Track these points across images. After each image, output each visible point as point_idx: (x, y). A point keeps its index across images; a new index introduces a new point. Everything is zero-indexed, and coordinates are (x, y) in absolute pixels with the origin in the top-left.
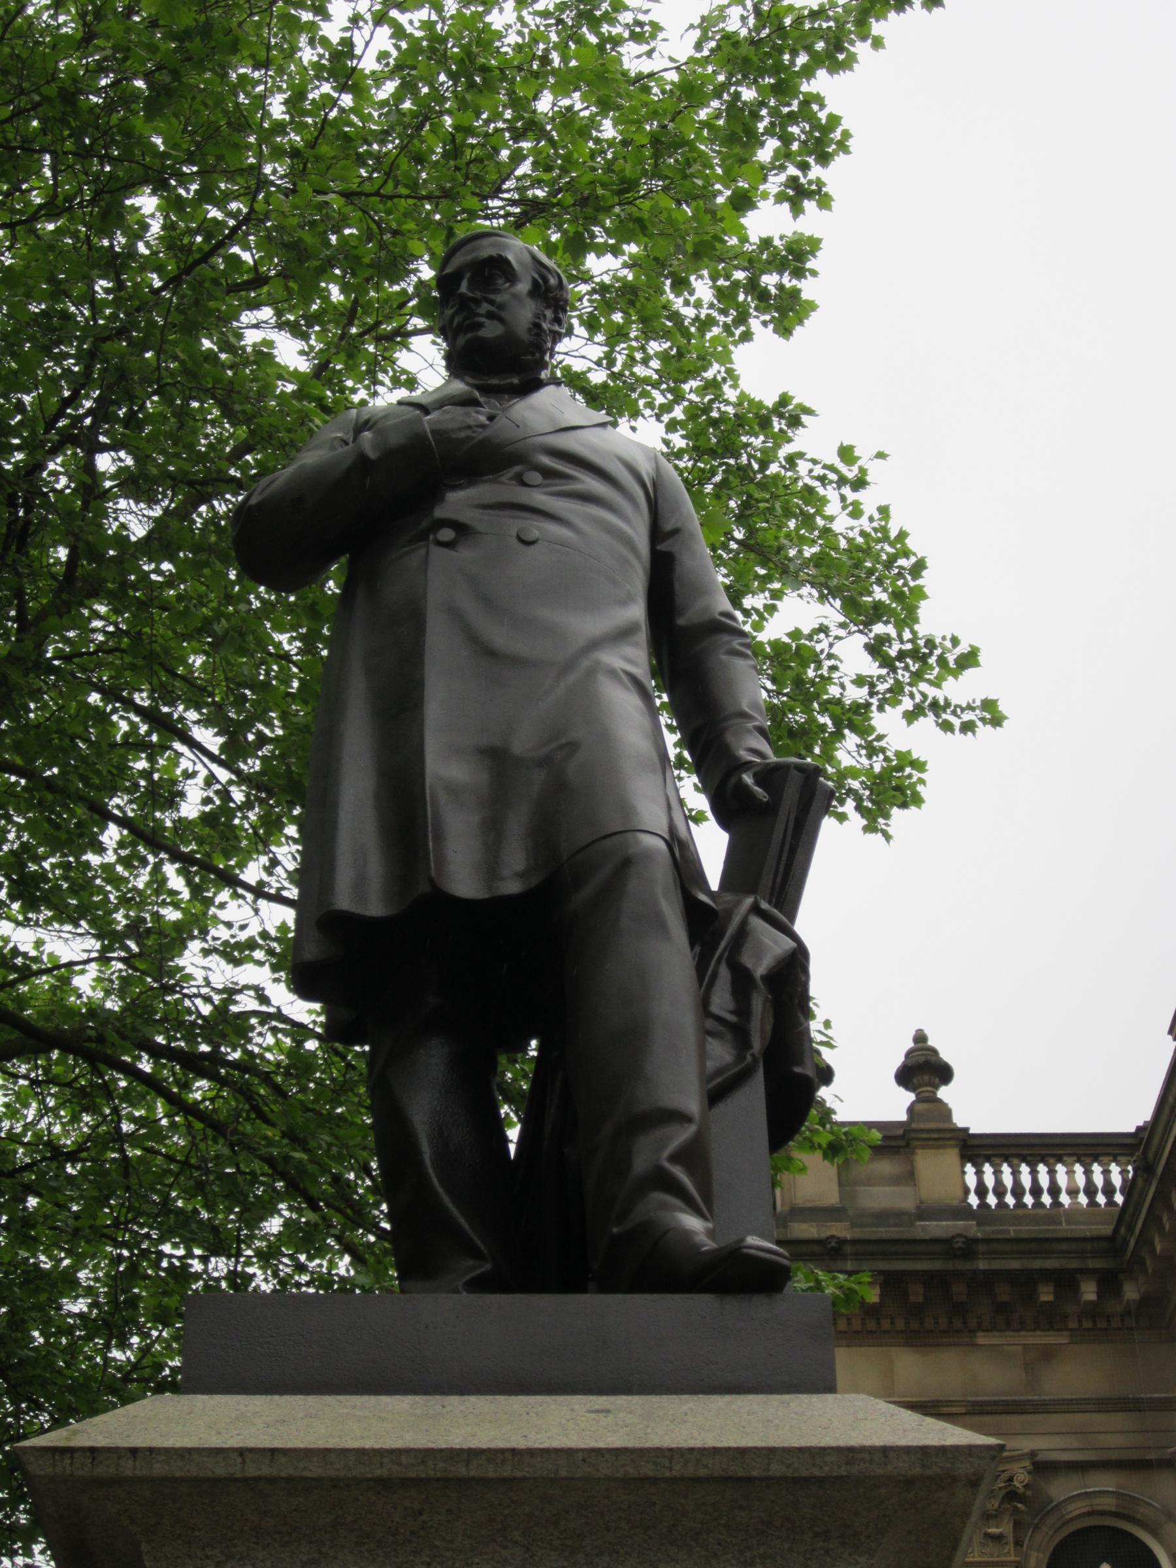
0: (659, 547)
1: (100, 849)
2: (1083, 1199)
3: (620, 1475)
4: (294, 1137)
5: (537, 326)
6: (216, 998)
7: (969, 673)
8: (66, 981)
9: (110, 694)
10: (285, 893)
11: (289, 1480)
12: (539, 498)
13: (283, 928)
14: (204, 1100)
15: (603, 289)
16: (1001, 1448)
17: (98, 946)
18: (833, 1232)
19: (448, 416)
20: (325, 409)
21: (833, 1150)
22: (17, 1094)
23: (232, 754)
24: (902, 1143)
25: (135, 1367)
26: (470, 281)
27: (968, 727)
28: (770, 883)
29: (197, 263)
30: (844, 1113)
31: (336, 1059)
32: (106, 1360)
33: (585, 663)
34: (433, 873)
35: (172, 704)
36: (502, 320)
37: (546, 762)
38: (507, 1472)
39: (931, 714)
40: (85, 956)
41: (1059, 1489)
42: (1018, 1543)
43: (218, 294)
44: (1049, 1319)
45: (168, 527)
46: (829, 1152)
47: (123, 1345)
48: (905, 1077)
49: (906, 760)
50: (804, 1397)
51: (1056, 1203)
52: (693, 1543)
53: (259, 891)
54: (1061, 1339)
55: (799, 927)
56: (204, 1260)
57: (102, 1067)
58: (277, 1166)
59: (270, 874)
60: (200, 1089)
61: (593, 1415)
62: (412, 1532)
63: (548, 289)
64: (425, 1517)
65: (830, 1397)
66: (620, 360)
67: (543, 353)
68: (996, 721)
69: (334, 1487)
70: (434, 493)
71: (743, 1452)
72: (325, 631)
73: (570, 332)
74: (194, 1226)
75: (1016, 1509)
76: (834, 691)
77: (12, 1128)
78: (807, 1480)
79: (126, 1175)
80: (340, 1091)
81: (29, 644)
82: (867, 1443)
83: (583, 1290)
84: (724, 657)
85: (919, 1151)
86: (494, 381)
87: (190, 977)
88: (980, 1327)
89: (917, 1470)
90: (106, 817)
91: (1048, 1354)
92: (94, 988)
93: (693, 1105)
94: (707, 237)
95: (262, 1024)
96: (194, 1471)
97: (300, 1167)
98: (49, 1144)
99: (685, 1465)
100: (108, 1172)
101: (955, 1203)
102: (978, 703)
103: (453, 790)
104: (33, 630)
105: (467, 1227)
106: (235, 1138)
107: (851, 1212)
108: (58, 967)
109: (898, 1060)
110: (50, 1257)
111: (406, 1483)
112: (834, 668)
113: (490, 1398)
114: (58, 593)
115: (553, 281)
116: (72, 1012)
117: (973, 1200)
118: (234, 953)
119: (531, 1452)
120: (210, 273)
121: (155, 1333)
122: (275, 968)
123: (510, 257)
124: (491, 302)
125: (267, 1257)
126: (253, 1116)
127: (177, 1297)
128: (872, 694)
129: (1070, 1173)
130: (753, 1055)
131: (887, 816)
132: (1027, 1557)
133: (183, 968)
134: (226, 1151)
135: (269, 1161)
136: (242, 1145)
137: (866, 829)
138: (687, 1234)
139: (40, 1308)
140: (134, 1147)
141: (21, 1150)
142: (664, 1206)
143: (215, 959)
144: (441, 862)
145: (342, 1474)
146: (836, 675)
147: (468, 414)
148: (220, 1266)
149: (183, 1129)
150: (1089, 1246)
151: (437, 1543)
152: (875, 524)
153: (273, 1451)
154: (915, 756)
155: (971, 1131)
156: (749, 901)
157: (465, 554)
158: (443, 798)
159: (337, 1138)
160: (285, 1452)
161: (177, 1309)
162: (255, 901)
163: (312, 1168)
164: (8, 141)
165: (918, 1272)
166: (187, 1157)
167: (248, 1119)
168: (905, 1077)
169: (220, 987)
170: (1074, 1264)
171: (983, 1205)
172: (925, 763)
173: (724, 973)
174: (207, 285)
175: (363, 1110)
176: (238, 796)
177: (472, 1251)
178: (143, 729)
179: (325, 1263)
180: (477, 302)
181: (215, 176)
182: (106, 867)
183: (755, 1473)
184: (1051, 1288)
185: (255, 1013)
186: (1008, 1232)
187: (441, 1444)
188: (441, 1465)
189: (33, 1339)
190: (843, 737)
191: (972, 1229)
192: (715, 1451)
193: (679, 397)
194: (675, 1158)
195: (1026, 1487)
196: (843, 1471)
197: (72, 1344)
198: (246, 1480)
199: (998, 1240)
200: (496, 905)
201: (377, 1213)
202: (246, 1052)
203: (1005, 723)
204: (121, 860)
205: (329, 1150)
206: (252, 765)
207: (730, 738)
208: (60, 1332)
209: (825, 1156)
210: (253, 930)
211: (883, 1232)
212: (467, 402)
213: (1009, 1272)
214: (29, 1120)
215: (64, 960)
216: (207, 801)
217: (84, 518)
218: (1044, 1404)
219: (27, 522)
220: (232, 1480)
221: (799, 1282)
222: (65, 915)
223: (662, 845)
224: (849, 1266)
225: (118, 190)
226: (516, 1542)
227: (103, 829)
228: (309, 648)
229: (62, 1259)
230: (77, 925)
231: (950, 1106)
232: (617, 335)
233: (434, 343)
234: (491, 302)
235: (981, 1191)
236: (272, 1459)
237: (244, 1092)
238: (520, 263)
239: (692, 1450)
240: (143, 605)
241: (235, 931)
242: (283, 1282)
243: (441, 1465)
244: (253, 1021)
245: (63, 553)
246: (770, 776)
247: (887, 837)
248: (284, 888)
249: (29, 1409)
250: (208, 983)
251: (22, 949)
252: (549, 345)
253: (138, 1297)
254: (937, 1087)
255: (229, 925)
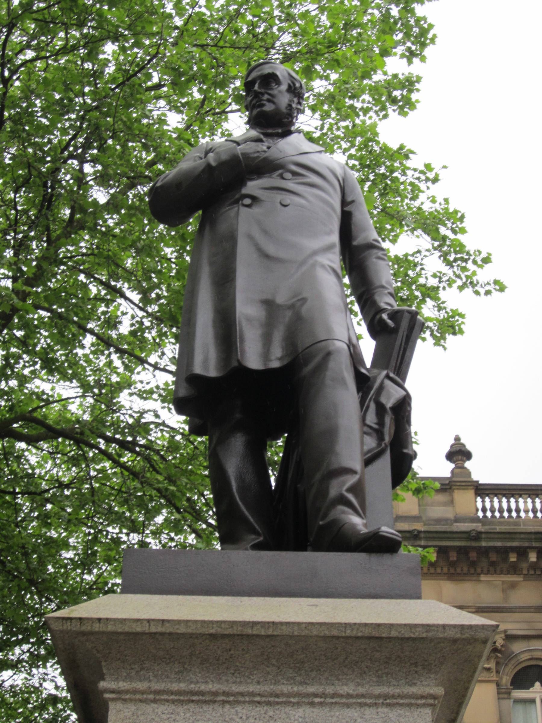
0: (345, 209)
1: (83, 347)
2: (531, 515)
3: (322, 634)
4: (170, 479)
5: (290, 105)
6: (136, 415)
7: (487, 266)
8: (65, 407)
9: (89, 275)
10: (167, 368)
11: (170, 634)
12: (290, 185)
13: (167, 384)
14: (128, 462)
15: (319, 95)
16: (497, 626)
17: (82, 391)
18: (416, 528)
19: (249, 147)
20: (191, 145)
21: (417, 491)
22: (42, 457)
23: (146, 300)
24: (448, 487)
25: (95, 583)
26: (259, 84)
27: (488, 293)
28: (394, 365)
29: (132, 76)
30: (422, 473)
31: (189, 444)
32: (82, 580)
33: (311, 261)
34: (239, 357)
35: (117, 281)
36: (274, 103)
37: (292, 307)
38: (270, 632)
39: (470, 287)
40: (75, 395)
41: (517, 647)
42: (498, 672)
43: (142, 91)
44: (514, 569)
45: (117, 198)
46: (416, 492)
47: (90, 572)
48: (451, 456)
49: (456, 313)
50: (407, 601)
51: (519, 516)
52: (355, 667)
53: (156, 367)
54: (519, 579)
55: (407, 385)
56: (128, 535)
57: (82, 446)
58: (162, 493)
59: (161, 359)
60: (127, 458)
61: (310, 607)
62: (226, 659)
63: (295, 89)
64: (232, 652)
65: (419, 601)
66: (326, 126)
67: (293, 118)
68: (502, 288)
69: (191, 637)
70: (242, 183)
71: (379, 625)
72: (188, 248)
73: (303, 112)
74: (123, 520)
75: (497, 656)
76: (422, 281)
77: (40, 473)
78: (408, 639)
79: (93, 495)
80: (192, 458)
81: (52, 251)
82: (436, 622)
83: (305, 549)
84: (374, 260)
85: (456, 491)
86: (270, 131)
87: (123, 406)
88: (482, 572)
89: (458, 636)
90: (85, 330)
91: (513, 586)
92: (78, 409)
93: (357, 464)
94: (368, 69)
95: (156, 427)
96: (127, 629)
97: (173, 494)
98: (57, 480)
99: (352, 630)
100: (84, 494)
101: (472, 515)
102: (491, 282)
103: (249, 319)
104: (54, 245)
105: (252, 520)
106: (143, 480)
107: (424, 518)
108: (62, 400)
109: (447, 449)
110: (57, 532)
111: (224, 636)
112: (422, 269)
113: (263, 598)
114: (65, 228)
115: (298, 85)
116: (68, 421)
117: (480, 514)
118: (145, 395)
119: (281, 624)
120: (138, 82)
121: (104, 568)
122: (163, 401)
123: (278, 73)
124: (269, 94)
125: (156, 534)
126: (151, 470)
127: (114, 552)
128: (440, 282)
129: (525, 502)
130: (385, 444)
131: (445, 339)
132: (501, 679)
133: (120, 402)
134: (139, 486)
135: (159, 490)
136: (145, 482)
137: (435, 344)
138: (354, 526)
139: (53, 556)
140: (96, 482)
141: (44, 483)
142: (343, 512)
143: (135, 397)
144: (243, 352)
145: (194, 632)
146: (423, 272)
147: (258, 146)
148: (135, 538)
149: (120, 475)
150: (533, 536)
151: (238, 664)
152: (442, 207)
153: (163, 621)
154: (460, 311)
155: (480, 482)
156: (384, 373)
157: (256, 210)
158: (244, 323)
159: (189, 479)
160: (169, 621)
161: (114, 557)
162: (154, 371)
163: (178, 494)
164: (46, 19)
165: (454, 546)
166: (121, 487)
167: (149, 471)
168: (451, 456)
169: (137, 410)
170: (526, 544)
171: (485, 516)
172: (464, 315)
173: (373, 406)
174: (136, 86)
175: (201, 468)
176: (147, 322)
177: (254, 532)
178: (103, 292)
179: (182, 538)
180: (263, 94)
181: (141, 36)
182: (85, 355)
183: (384, 635)
184: (515, 555)
185: (153, 423)
186: (496, 529)
187: (240, 619)
188: (240, 628)
189: (48, 570)
190: (426, 301)
191: (479, 527)
192: (366, 625)
193: (353, 146)
194: (349, 490)
195: (502, 646)
196: (424, 635)
197: (66, 572)
198: (150, 634)
199: (491, 533)
200: (268, 373)
201: (206, 515)
202: (148, 440)
203: (506, 290)
204: (93, 352)
205: (186, 485)
206: (153, 308)
207: (377, 298)
208: (61, 567)
209: (414, 494)
210: (153, 385)
211: (439, 528)
212: (258, 140)
213: (495, 547)
214: (48, 469)
215: (64, 397)
216: (132, 325)
217: (78, 193)
218: (511, 608)
219: (52, 195)
220: (144, 633)
221: (402, 551)
222: (65, 377)
223: (346, 347)
224: (423, 543)
225: (96, 42)
226: (274, 665)
227: (85, 337)
228: (180, 257)
229: (62, 533)
230: (71, 382)
231: (471, 470)
232: (325, 116)
233: (241, 117)
234: (269, 94)
235: (484, 510)
236: (163, 625)
237: (148, 459)
238: (283, 76)
239: (355, 624)
240: (104, 234)
241: (144, 385)
242: (164, 546)
243: (240, 628)
244: (152, 426)
245: (68, 212)
246: (395, 315)
247: (445, 348)
248: (167, 365)
249: (46, 601)
250: (131, 409)
251: (46, 392)
252: (295, 114)
253: (97, 551)
254: (465, 462)
255: (142, 382)
